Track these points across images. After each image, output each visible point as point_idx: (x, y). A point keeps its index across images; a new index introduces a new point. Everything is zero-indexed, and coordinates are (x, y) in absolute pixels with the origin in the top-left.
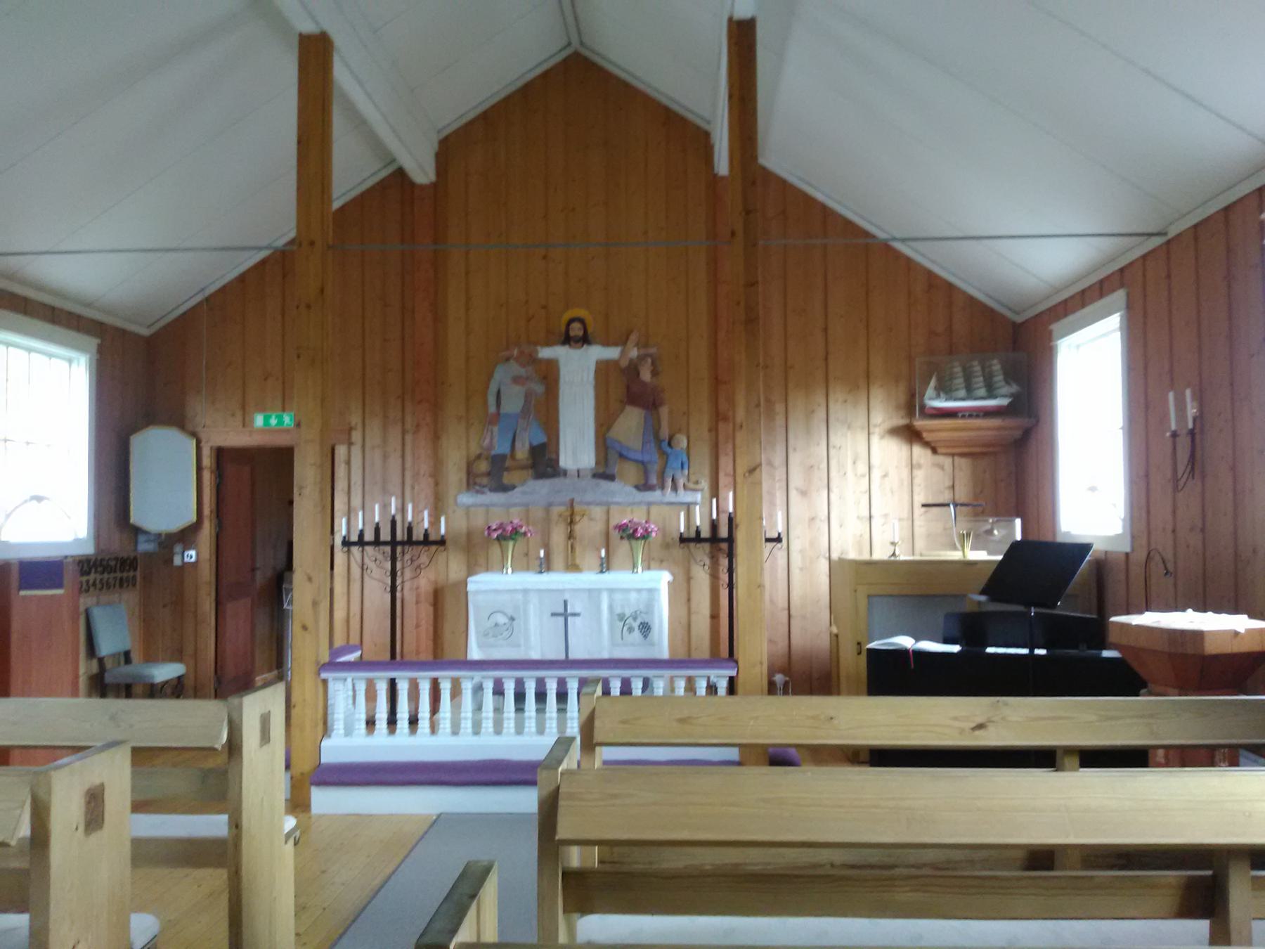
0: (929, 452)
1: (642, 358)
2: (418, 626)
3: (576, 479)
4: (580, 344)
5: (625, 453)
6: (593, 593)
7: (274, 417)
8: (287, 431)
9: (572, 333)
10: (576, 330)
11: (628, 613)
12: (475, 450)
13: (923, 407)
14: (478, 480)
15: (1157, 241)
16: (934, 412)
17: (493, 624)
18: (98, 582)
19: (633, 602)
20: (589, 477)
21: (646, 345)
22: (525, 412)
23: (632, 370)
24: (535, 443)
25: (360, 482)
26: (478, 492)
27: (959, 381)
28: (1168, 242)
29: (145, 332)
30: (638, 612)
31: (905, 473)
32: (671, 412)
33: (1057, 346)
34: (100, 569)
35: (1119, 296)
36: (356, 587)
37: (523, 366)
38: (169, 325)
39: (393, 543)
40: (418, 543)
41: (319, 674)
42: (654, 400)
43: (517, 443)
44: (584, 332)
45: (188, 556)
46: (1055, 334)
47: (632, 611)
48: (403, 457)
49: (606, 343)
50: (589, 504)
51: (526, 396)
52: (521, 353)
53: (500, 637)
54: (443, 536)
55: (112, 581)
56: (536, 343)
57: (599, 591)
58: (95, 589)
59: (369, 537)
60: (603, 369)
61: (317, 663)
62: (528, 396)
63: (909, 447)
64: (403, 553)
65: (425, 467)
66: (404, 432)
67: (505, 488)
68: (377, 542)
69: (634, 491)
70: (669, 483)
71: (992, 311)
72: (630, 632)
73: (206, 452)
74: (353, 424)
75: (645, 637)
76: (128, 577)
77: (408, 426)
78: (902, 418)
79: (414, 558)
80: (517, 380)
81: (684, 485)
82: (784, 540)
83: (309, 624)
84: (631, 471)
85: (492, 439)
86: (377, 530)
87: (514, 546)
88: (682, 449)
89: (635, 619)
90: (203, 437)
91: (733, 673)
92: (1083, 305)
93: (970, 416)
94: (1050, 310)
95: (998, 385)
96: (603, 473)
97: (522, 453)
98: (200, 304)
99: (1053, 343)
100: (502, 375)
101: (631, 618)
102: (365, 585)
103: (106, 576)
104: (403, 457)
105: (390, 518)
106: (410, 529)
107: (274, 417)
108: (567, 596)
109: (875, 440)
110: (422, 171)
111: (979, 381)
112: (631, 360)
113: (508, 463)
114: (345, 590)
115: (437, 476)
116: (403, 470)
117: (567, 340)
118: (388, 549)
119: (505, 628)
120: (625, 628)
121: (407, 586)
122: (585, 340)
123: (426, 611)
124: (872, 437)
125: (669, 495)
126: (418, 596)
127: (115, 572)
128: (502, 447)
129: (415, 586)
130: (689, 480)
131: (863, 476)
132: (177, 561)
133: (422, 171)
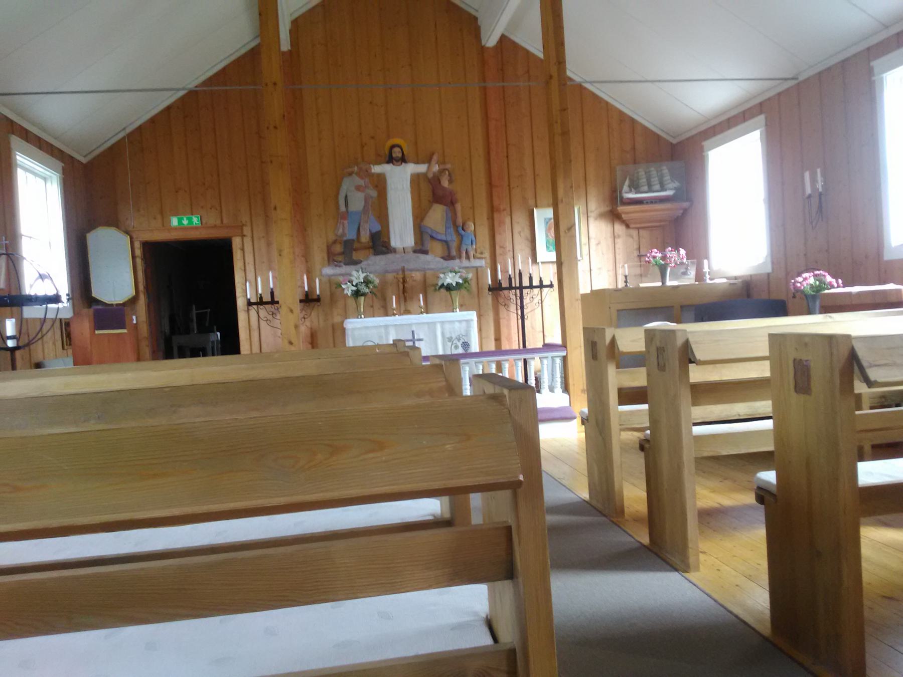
0: (624, 227)
1: (442, 171)
3: (403, 254)
4: (400, 163)
5: (434, 235)
6: (432, 325)
7: (185, 219)
8: (196, 228)
9: (394, 155)
11: (454, 337)
12: (332, 237)
13: (622, 198)
15: (793, 83)
16: (628, 201)
19: (459, 329)
20: (412, 252)
21: (444, 163)
22: (365, 210)
23: (434, 182)
24: (374, 231)
25: (252, 263)
26: (336, 266)
27: (643, 181)
28: (798, 84)
29: (84, 160)
30: (461, 336)
31: (610, 241)
33: (708, 155)
35: (761, 118)
36: (255, 335)
37: (362, 178)
38: (99, 156)
46: (876, 70)
47: (457, 335)
52: (360, 169)
54: (318, 296)
56: (370, 163)
57: (434, 323)
59: (267, 298)
60: (416, 180)
69: (442, 260)
70: (464, 254)
71: (658, 137)
73: (137, 245)
74: (244, 222)
79: (268, 322)
80: (358, 188)
84: (438, 248)
85: (343, 230)
87: (365, 299)
89: (459, 340)
90: (134, 236)
91: (564, 354)
92: (729, 128)
93: (652, 202)
96: (420, 249)
97: (365, 238)
98: (124, 138)
99: (704, 154)
100: (348, 185)
105: (270, 291)
107: (185, 219)
108: (414, 328)
109: (591, 220)
112: (434, 174)
113: (356, 245)
114: (248, 337)
115: (306, 256)
117: (391, 160)
120: (453, 346)
122: (403, 160)
124: (589, 219)
125: (465, 263)
128: (351, 235)
130: (476, 252)
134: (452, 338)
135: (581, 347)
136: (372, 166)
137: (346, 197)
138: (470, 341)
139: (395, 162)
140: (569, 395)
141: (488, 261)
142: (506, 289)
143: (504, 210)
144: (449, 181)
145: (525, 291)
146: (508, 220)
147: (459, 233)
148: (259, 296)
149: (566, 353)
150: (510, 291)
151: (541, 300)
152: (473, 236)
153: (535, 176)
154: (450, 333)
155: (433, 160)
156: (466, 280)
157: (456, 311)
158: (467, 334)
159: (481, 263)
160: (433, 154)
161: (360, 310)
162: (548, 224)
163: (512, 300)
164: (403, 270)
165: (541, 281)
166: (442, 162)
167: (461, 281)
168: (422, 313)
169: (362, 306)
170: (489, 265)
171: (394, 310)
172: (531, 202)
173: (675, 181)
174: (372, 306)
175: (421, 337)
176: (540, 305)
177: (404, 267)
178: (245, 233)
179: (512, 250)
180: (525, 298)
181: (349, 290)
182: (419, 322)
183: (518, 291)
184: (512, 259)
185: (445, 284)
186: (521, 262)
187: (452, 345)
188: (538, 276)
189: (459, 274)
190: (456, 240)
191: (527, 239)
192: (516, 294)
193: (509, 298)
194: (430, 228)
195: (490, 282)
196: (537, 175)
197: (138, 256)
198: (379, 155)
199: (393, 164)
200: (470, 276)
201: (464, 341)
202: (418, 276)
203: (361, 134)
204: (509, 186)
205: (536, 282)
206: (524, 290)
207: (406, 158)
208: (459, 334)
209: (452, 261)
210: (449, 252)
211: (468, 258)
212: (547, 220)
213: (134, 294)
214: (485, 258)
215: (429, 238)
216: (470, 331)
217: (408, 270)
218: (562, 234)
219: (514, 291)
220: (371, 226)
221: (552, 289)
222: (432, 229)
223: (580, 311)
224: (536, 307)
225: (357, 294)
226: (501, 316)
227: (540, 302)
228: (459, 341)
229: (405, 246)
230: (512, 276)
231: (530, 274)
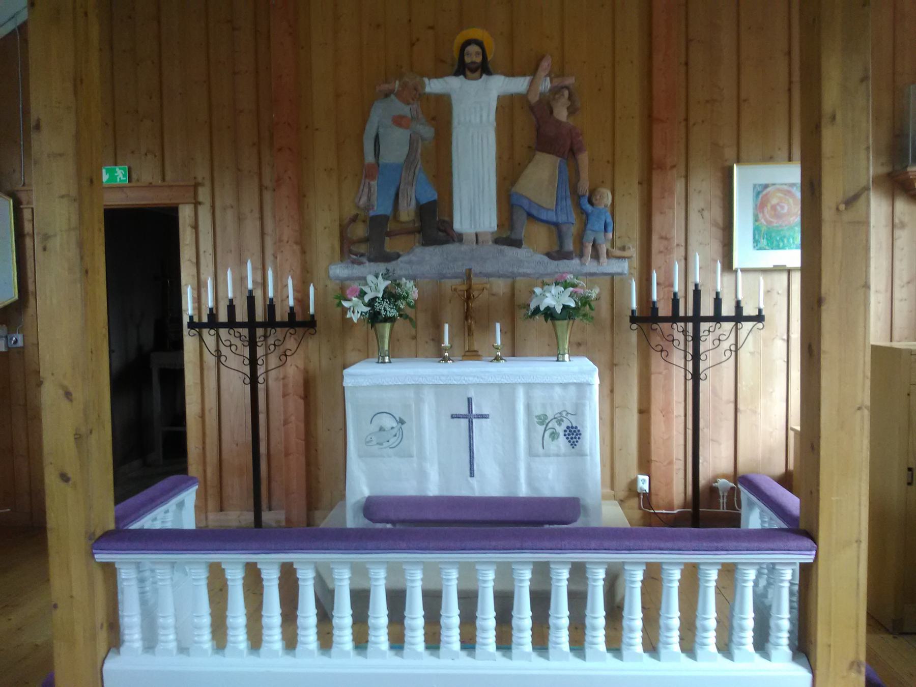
1: (556, 91)
2: (286, 422)
4: (477, 74)
5: (535, 212)
6: (506, 390)
8: (120, 188)
9: (468, 60)
11: (550, 415)
14: (354, 248)
17: (378, 429)
19: (560, 400)
20: (490, 243)
21: (562, 74)
22: (410, 161)
24: (424, 201)
25: (210, 250)
26: (354, 262)
30: (564, 414)
32: (592, 160)
39: (252, 324)
40: (282, 325)
41: (93, 554)
42: (572, 143)
43: (400, 201)
44: (483, 57)
48: (262, 218)
49: (511, 73)
50: (488, 275)
51: (411, 143)
52: (404, 86)
53: (386, 444)
54: (313, 316)
57: (513, 386)
59: (223, 317)
61: (90, 536)
63: (890, 202)
64: (266, 337)
65: (288, 233)
66: (261, 188)
67: (388, 258)
68: (232, 323)
69: (546, 259)
72: (553, 439)
74: (200, 180)
75: (573, 445)
77: (267, 182)
78: (882, 164)
80: (399, 121)
81: (607, 250)
83: (71, 472)
84: (541, 235)
85: (369, 199)
86: (231, 308)
88: (606, 206)
89: (560, 422)
91: (808, 558)
97: (407, 213)
100: (380, 114)
101: (554, 421)
102: (222, 375)
104: (262, 218)
108: (472, 394)
113: (391, 226)
114: (199, 381)
115: (303, 242)
116: (263, 234)
117: (462, 69)
118: (245, 332)
121: (272, 374)
122: (484, 69)
123: (295, 405)
125: (590, 266)
126: (285, 386)
128: (382, 207)
129: (281, 376)
135: (859, 541)
136: (426, 80)
138: (583, 427)
139: (468, 73)
140: (813, 671)
141: (636, 262)
142: (665, 319)
143: (673, 167)
144: (568, 108)
145: (704, 326)
146: (679, 186)
147: (582, 209)
148: (268, 303)
149: (813, 557)
150: (675, 325)
151: (736, 344)
152: (609, 214)
153: (739, 102)
154: (544, 406)
155: (540, 69)
156: (585, 301)
157: (563, 361)
158: (579, 409)
159: (623, 267)
160: (540, 59)
161: (383, 348)
162: (760, 196)
163: (676, 343)
164: (468, 275)
165: (738, 307)
166: (558, 72)
167: (573, 305)
168: (497, 359)
169: (387, 340)
170: (636, 273)
171: (445, 349)
172: (730, 153)
174: (414, 338)
175: (485, 412)
176: (733, 353)
177: (470, 270)
178: (201, 198)
179: (683, 244)
180: (702, 339)
181: (356, 310)
182: (482, 381)
183: (690, 326)
184: (683, 262)
185: (542, 309)
186: (700, 268)
187: (545, 430)
188: (734, 296)
189: (571, 289)
190: (574, 222)
191: (715, 224)
192: (685, 332)
193: (671, 338)
194: (526, 198)
195: (634, 305)
196: (745, 101)
197: (28, 234)
198: (443, 61)
199: (466, 77)
200: (594, 293)
201: (570, 426)
202: (500, 286)
203: (410, 21)
204: (686, 120)
205: (727, 309)
206: (702, 324)
207: (490, 66)
208: (561, 410)
209: (565, 261)
210: (561, 245)
211: (596, 256)
212: (759, 189)
213: (17, 297)
214: (629, 258)
215: (525, 215)
216: (584, 405)
217: (481, 274)
218: (827, 214)
219: (683, 324)
221: (760, 325)
222: (530, 201)
223: (866, 442)
224: (724, 358)
225: (375, 318)
226: (653, 368)
227: (733, 348)
228: (560, 424)
229: (479, 230)
230: (681, 296)
231: (717, 294)
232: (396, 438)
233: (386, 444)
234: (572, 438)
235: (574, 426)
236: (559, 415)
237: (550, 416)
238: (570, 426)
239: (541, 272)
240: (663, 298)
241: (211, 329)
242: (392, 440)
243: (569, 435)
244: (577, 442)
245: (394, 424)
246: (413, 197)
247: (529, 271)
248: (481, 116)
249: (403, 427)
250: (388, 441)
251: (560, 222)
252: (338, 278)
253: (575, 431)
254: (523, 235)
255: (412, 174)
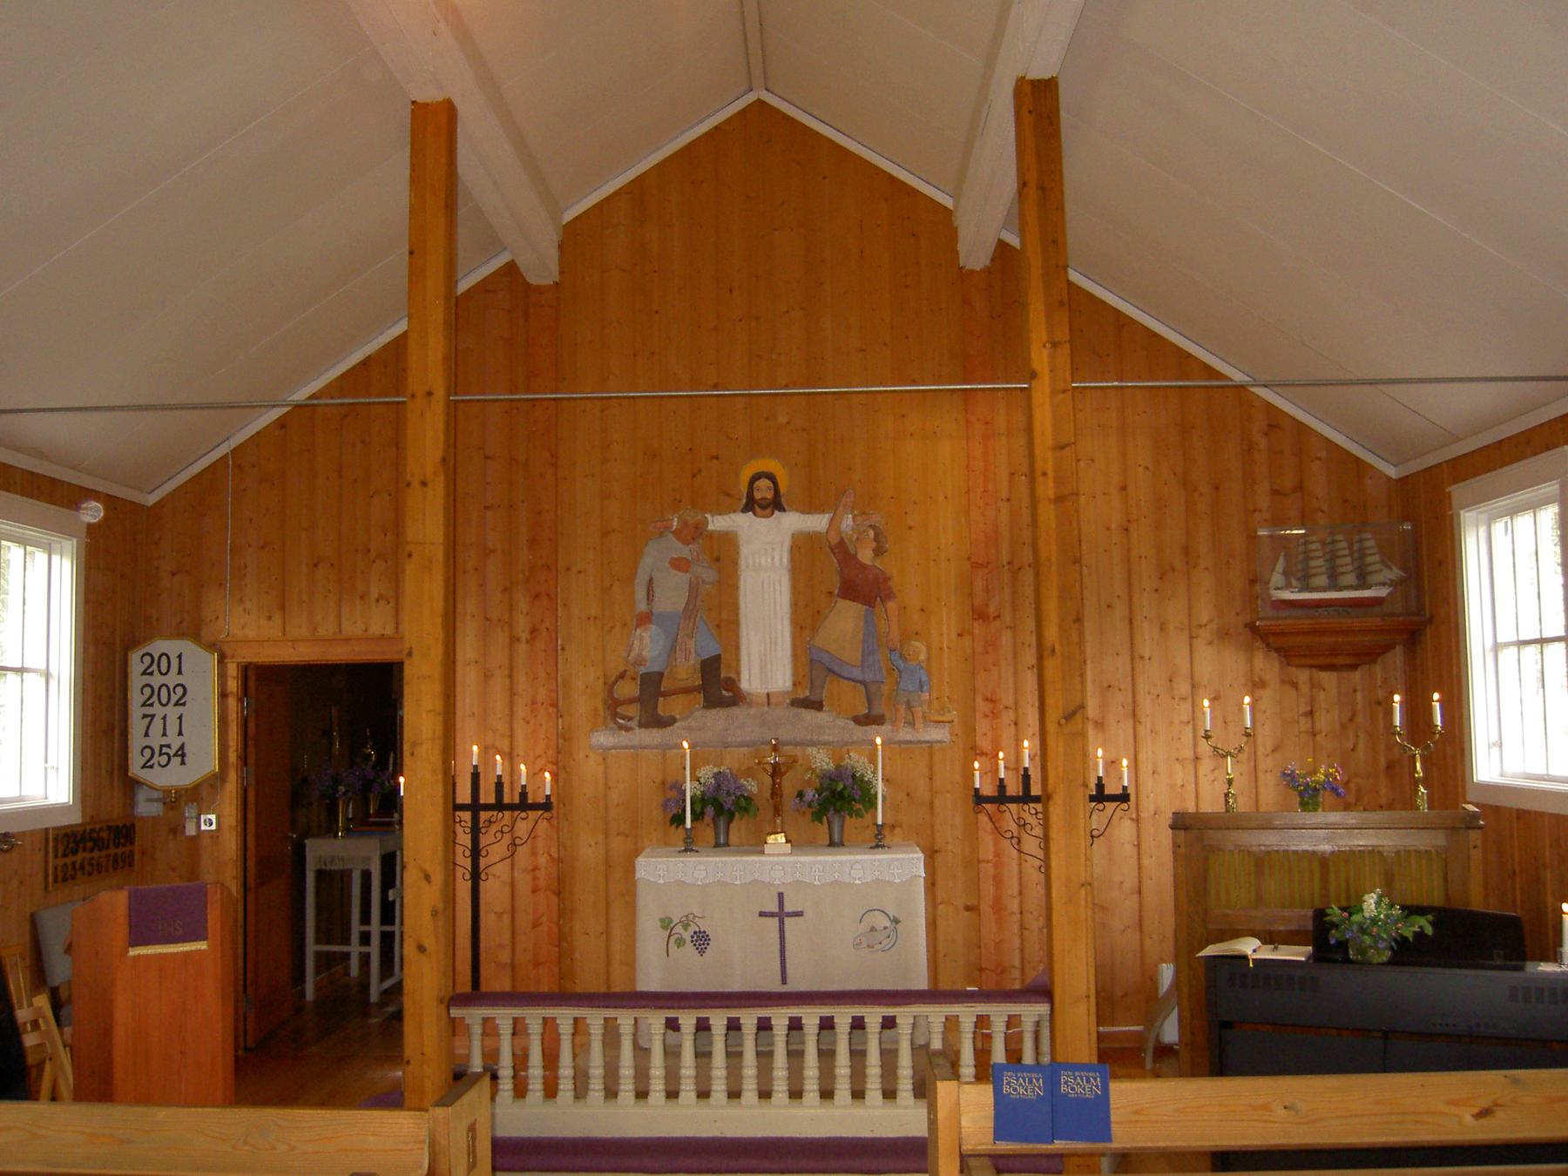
3: (766, 709)
4: (769, 511)
5: (836, 669)
9: (758, 496)
10: (763, 490)
12: (616, 667)
18: (86, 862)
22: (690, 610)
26: (621, 727)
30: (691, 917)
34: (89, 844)
39: (475, 807)
45: (205, 821)
52: (684, 524)
53: (878, 947)
54: (548, 797)
55: (104, 862)
58: (84, 874)
59: (1013, 788)
60: (803, 547)
62: (694, 589)
66: (514, 640)
69: (852, 724)
73: (232, 670)
76: (123, 853)
80: (679, 564)
82: (1132, 798)
89: (686, 927)
94: (1454, 462)
95: (1371, 569)
97: (686, 670)
98: (224, 459)
103: (96, 854)
106: (499, 786)
109: (1199, 644)
110: (542, 266)
111: (1346, 564)
116: (513, 693)
117: (751, 505)
119: (885, 933)
120: (672, 939)
127: (108, 847)
131: (1184, 699)
132: (190, 830)
133: (542, 266)
134: (671, 921)
137: (651, 580)
145: (484, 815)
173: (1393, 567)
187: (670, 936)
197: (232, 693)
199: (755, 514)
220: (705, 644)
228: (686, 929)
229: (770, 689)
232: (888, 940)
233: (878, 947)
234: (700, 945)
235: (702, 930)
236: (684, 919)
237: (676, 920)
238: (698, 930)
239: (846, 739)
240: (991, 771)
241: (1024, 804)
242: (884, 943)
243: (697, 941)
244: (706, 948)
245: (888, 924)
246: (693, 651)
247: (831, 739)
248: (773, 559)
249: (898, 926)
250: (880, 943)
251: (868, 681)
252: (601, 747)
253: (703, 937)
254: (824, 695)
255: (691, 625)
